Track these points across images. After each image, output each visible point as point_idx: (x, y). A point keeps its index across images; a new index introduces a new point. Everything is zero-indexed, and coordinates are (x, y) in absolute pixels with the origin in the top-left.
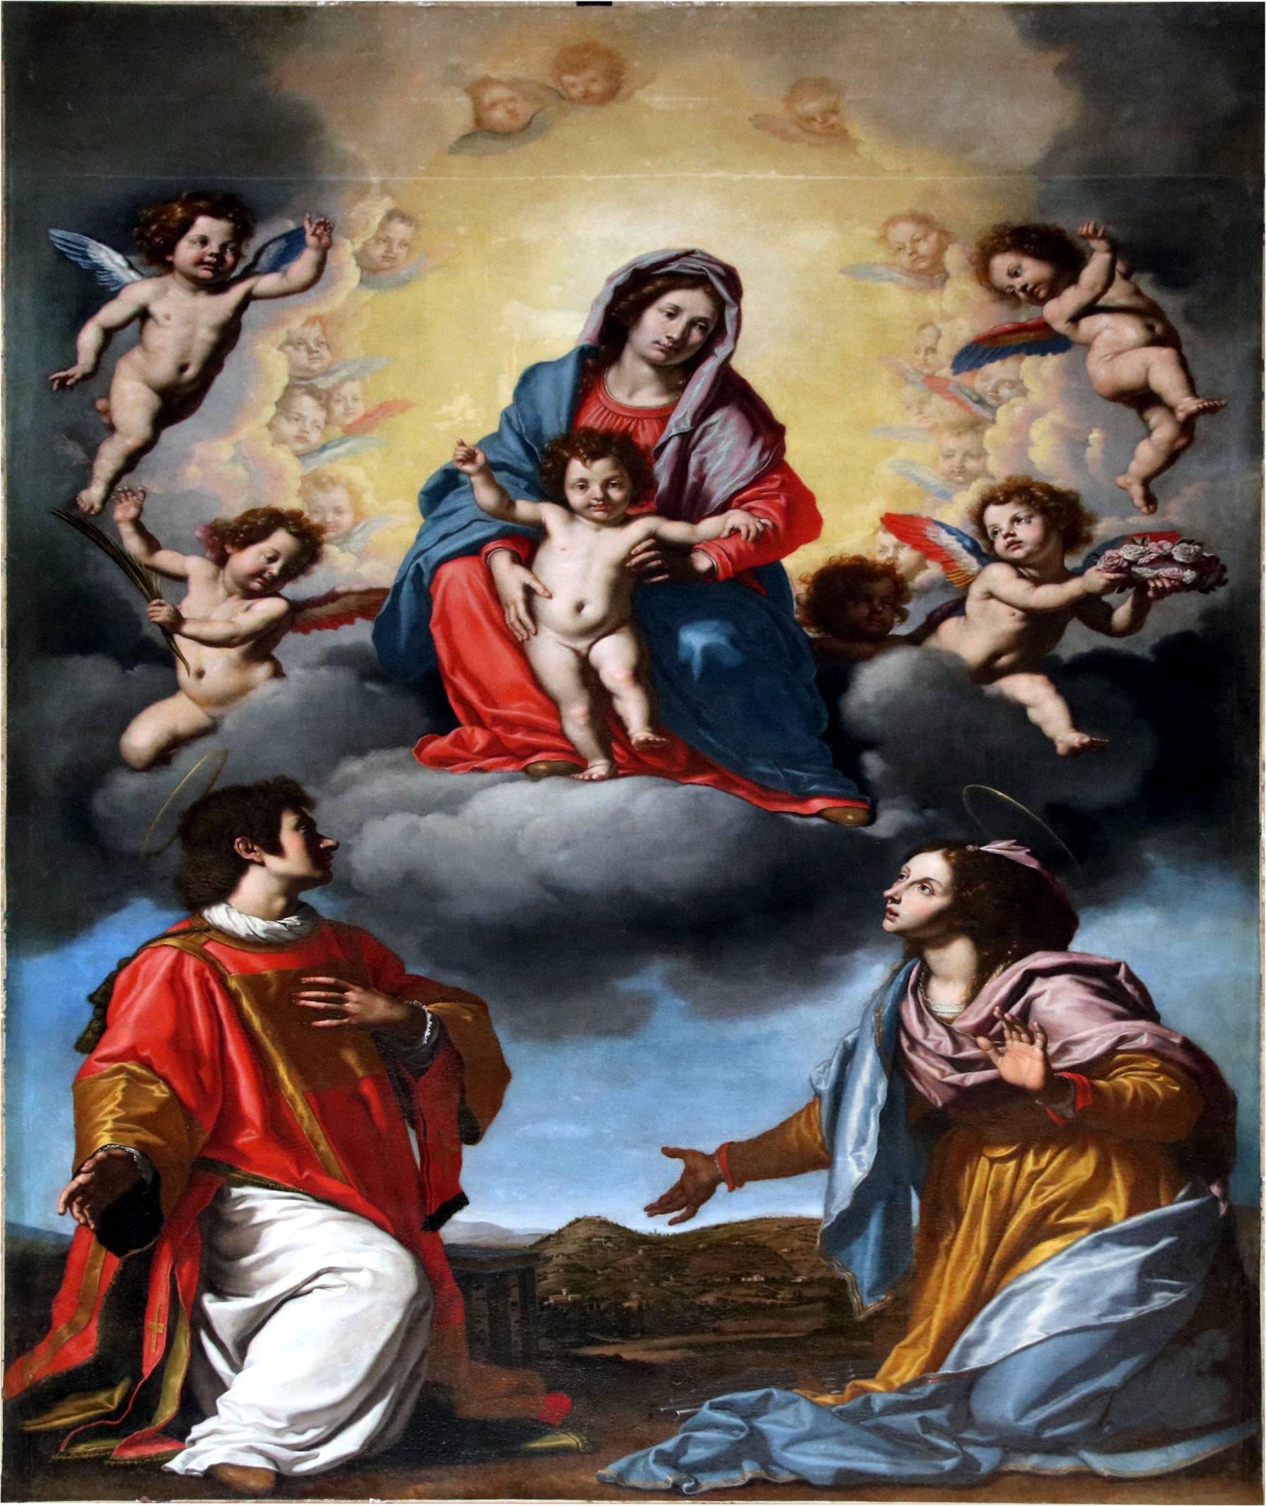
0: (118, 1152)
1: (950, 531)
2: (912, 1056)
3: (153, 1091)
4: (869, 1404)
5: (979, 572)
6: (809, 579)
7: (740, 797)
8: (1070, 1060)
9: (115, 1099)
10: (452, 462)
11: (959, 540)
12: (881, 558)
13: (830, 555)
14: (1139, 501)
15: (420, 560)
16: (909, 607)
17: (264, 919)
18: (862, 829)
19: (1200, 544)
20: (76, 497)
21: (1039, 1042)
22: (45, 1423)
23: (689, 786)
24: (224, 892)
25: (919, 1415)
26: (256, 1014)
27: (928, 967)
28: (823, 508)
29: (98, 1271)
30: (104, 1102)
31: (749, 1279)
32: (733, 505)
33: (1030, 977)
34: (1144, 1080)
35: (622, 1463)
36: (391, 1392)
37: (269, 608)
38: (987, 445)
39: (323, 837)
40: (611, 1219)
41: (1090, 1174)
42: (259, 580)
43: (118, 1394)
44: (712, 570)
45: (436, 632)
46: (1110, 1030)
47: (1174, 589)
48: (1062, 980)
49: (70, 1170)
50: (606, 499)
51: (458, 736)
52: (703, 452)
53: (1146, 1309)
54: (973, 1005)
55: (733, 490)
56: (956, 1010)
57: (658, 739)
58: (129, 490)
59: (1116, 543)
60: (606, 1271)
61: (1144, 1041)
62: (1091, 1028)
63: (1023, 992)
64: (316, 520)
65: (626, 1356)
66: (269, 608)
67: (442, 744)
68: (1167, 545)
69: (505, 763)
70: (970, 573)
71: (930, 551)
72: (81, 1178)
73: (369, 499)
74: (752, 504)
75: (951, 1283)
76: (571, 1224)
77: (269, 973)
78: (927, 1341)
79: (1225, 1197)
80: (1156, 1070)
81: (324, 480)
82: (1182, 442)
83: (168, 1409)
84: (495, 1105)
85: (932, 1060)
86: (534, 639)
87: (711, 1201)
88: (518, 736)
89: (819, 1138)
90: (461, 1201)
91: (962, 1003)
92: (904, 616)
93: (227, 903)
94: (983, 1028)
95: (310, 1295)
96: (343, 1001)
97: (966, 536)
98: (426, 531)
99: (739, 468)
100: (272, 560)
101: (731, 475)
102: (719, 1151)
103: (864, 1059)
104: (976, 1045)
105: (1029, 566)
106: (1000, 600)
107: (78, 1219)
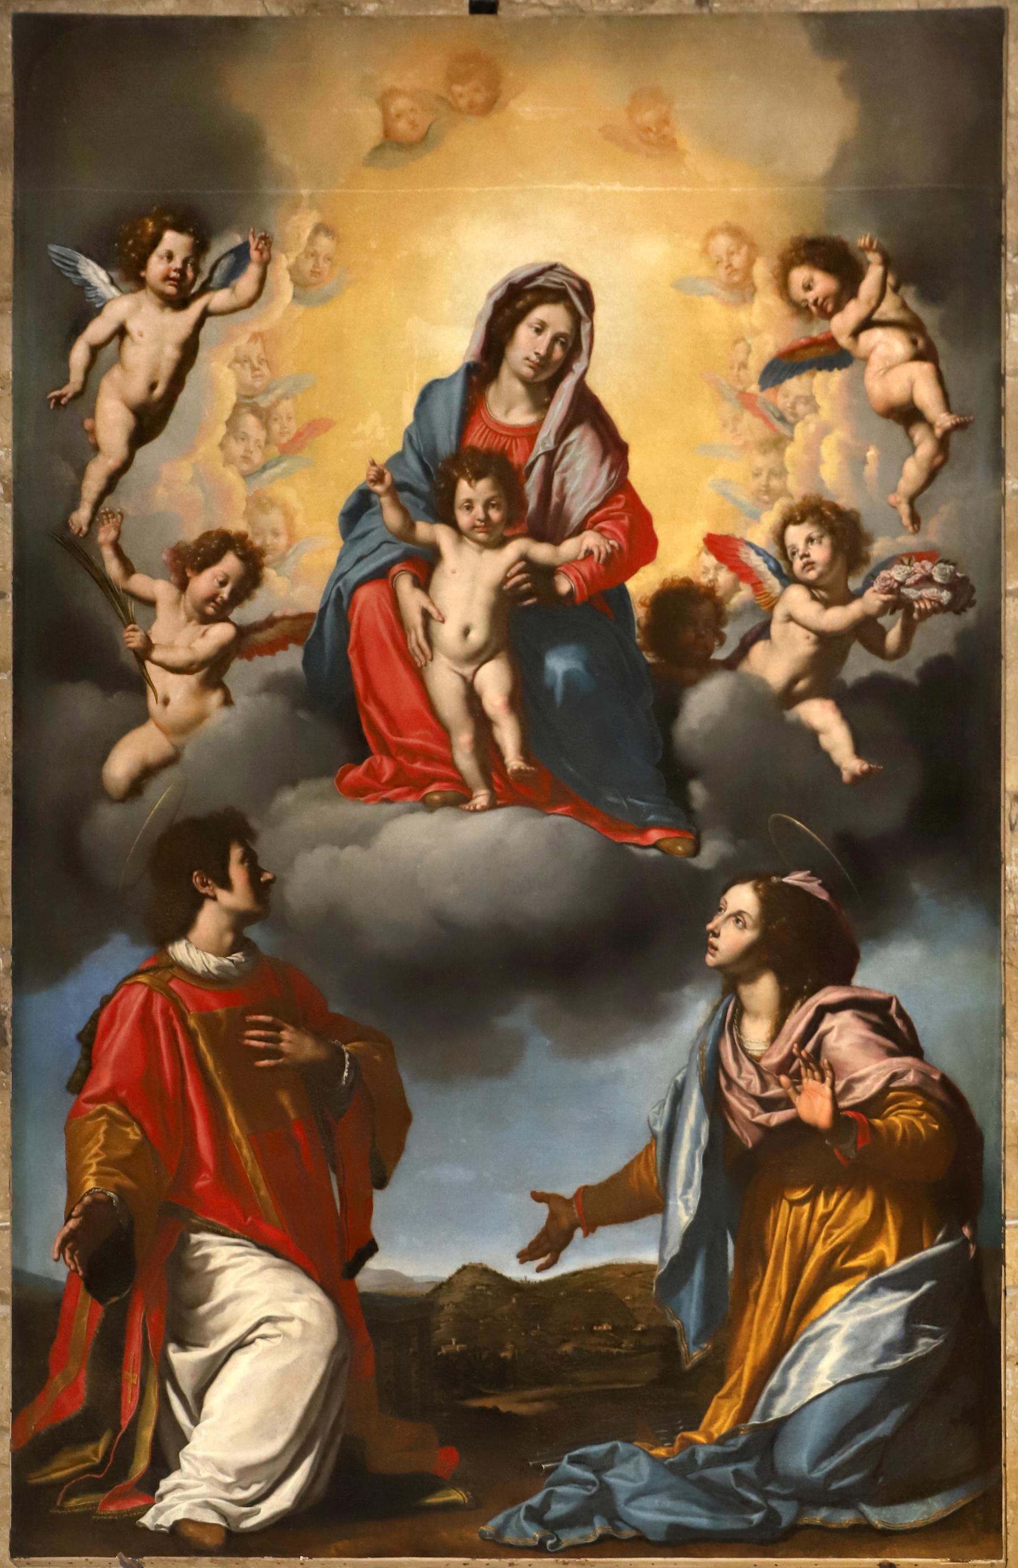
0: (100, 1196)
1: (759, 552)
3: (128, 1134)
5: (781, 594)
6: (648, 602)
8: (853, 1099)
10: (365, 483)
11: (766, 562)
12: (704, 580)
13: (664, 578)
14: (906, 520)
15: (340, 584)
16: (726, 630)
17: (217, 954)
19: (954, 564)
21: (828, 1080)
22: (45, 1475)
24: (183, 928)
26: (210, 1054)
28: (660, 529)
29: (85, 1319)
30: (90, 1144)
31: (600, 1328)
32: (587, 527)
33: (822, 1011)
35: (499, 1519)
39: (264, 871)
40: (492, 1266)
41: (868, 1217)
42: (212, 604)
43: (102, 1446)
44: (571, 593)
45: (353, 658)
46: (885, 1067)
47: (935, 611)
48: (846, 1016)
50: (487, 519)
51: (370, 764)
53: (912, 1355)
57: (528, 768)
58: (110, 512)
59: (887, 564)
61: (911, 1078)
63: (816, 1028)
64: (258, 542)
65: (504, 1408)
66: (221, 632)
67: (358, 772)
68: (928, 565)
69: (408, 794)
70: (773, 595)
71: (743, 573)
72: (72, 1223)
73: (299, 520)
74: (602, 525)
75: (759, 1330)
76: (459, 1272)
77: (220, 1011)
79: (974, 1238)
82: (939, 459)
83: (141, 1464)
84: (399, 1148)
85: (744, 1099)
86: (430, 664)
88: (418, 765)
89: (655, 1181)
90: (371, 1249)
92: (722, 639)
93: (186, 938)
94: (784, 1067)
95: (253, 1345)
97: (770, 556)
99: (592, 488)
100: (223, 584)
103: (691, 1098)
104: (779, 1084)
106: (798, 622)
107: (69, 1266)
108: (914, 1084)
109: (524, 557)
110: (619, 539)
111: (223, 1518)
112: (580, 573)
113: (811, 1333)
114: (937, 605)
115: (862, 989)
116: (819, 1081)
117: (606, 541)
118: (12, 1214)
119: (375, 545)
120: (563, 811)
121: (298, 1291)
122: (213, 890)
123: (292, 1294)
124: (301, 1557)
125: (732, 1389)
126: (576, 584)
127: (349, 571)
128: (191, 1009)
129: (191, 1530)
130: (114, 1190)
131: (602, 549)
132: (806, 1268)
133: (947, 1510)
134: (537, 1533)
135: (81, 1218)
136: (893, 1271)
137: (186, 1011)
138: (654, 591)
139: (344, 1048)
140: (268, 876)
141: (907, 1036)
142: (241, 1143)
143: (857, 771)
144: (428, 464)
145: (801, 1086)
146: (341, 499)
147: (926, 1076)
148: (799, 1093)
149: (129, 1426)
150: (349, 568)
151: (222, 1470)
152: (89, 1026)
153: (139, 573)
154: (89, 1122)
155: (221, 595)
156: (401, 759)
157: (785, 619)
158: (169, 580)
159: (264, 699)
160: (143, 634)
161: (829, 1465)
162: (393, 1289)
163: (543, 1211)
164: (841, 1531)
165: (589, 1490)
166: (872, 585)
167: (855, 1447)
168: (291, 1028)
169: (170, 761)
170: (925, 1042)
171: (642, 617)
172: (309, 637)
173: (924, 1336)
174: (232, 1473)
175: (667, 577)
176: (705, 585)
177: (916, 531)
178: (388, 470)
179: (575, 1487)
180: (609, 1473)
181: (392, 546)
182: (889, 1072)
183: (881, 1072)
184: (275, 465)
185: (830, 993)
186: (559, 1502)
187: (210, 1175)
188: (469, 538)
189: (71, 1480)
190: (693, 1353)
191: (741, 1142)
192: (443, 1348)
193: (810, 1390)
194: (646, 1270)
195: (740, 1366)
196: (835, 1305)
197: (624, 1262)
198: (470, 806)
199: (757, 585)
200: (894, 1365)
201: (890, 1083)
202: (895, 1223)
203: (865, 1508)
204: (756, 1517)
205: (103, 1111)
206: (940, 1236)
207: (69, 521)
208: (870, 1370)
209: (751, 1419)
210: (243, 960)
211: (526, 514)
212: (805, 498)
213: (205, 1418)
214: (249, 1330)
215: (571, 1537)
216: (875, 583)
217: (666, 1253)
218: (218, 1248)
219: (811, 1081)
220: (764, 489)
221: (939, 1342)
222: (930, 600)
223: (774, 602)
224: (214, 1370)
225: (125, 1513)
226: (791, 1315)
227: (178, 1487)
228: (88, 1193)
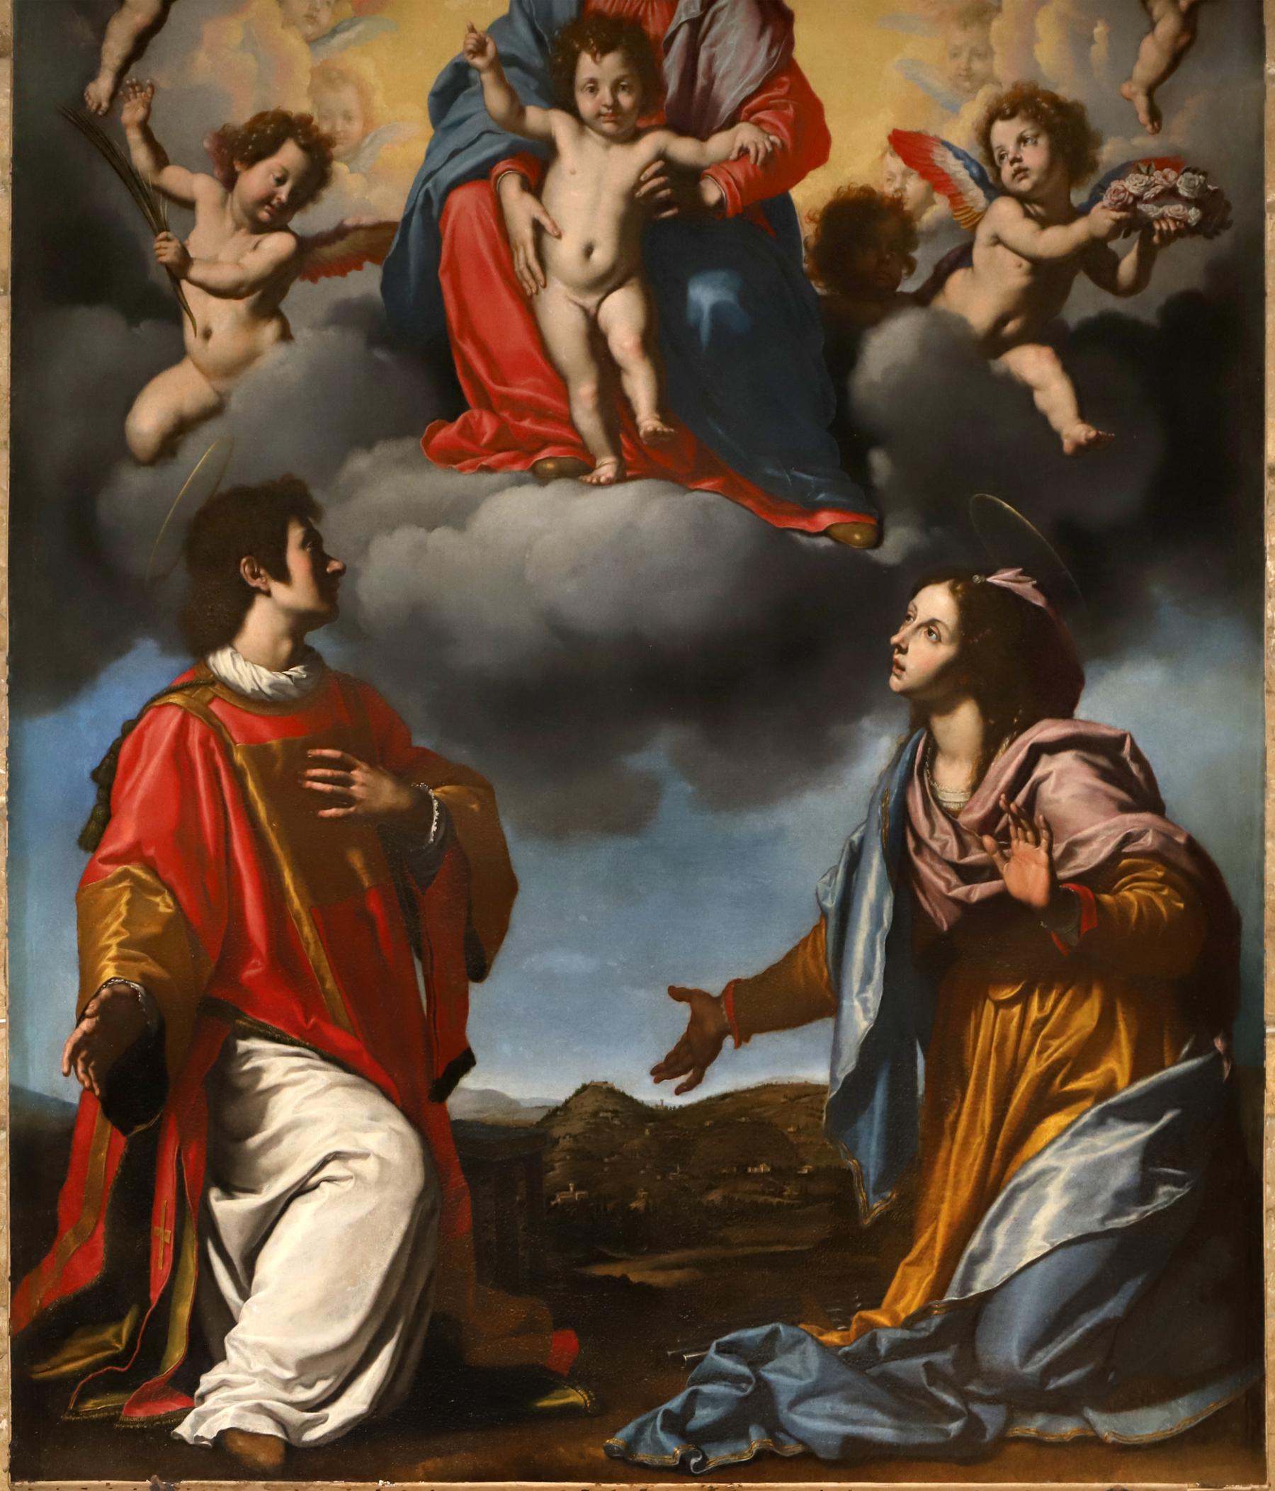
0: (123, 988)
1: (958, 155)
2: (918, 862)
3: (158, 905)
4: (875, 1344)
5: (986, 209)
6: (818, 216)
7: (746, 508)
8: (1075, 867)
9: (119, 915)
10: (462, 54)
11: (966, 167)
12: (889, 190)
13: (838, 185)
14: (1143, 117)
15: (429, 185)
16: (917, 254)
17: (269, 669)
18: (869, 552)
19: (1204, 174)
20: (83, 91)
21: (1044, 842)
22: (53, 1368)
23: (695, 493)
24: (227, 633)
25: (924, 1360)
26: (262, 800)
27: (934, 741)
28: (833, 123)
29: (103, 1154)
30: (109, 919)
31: (756, 1170)
32: (742, 118)
33: (1037, 752)
34: (1148, 894)
35: (629, 1430)
36: (400, 1327)
37: (277, 245)
38: (993, 41)
39: (332, 559)
40: (618, 1086)
41: (1094, 1024)
42: (267, 207)
43: (126, 1328)
44: (721, 203)
45: (445, 282)
46: (1115, 827)
47: (1179, 233)
48: (1067, 759)
49: (74, 1011)
50: (616, 105)
51: (466, 421)
52: (712, 45)
53: (1149, 1209)
54: (979, 791)
55: (741, 98)
56: (962, 799)
57: (666, 430)
58: (138, 84)
59: (1120, 172)
60: (613, 1159)
61: (1149, 841)
62: (1097, 823)
63: (1029, 775)
64: (325, 128)
65: (634, 1278)
66: (277, 245)
67: (450, 431)
68: (1172, 175)
69: (514, 461)
70: (976, 210)
71: (938, 181)
72: (86, 1025)
73: (378, 99)
74: (760, 115)
75: (957, 1174)
76: (578, 1093)
77: (274, 743)
78: (933, 1255)
79: (1228, 1049)
80: (1161, 880)
81: (334, 74)
82: (1183, 40)
83: (177, 1353)
84: (501, 928)
85: (938, 867)
86: (542, 292)
87: (716, 1061)
88: (526, 423)
89: (826, 974)
90: (466, 1061)
91: (968, 788)
92: (911, 266)
93: (232, 646)
94: (988, 824)
95: (317, 1191)
96: (348, 782)
97: (972, 161)
98: (490, 115)
99: (748, 67)
100: (281, 181)
101: (740, 78)
102: (725, 992)
103: (870, 865)
104: (982, 847)
105: (1037, 202)
106: (1006, 246)
107: (82, 1082)
108: (1153, 848)
109: (661, 156)
110: (783, 135)
111: (281, 1429)
112: (733, 178)
113: (1022, 1178)
114: (1182, 226)
115: (1087, 722)
116: (1032, 843)
117: (766, 136)
118: (8, 1012)
119: (473, 134)
120: (710, 487)
121: (374, 1118)
122: (265, 583)
123: (366, 1122)
124: (381, 1482)
125: (922, 1252)
126: (727, 190)
127: (439, 169)
128: (237, 741)
129: (240, 1443)
130: (139, 980)
131: (761, 146)
132: (1016, 1091)
133: (1196, 1417)
134: (679, 1448)
135: (98, 1018)
136: (1126, 1096)
137: (231, 742)
138: (826, 203)
139: (432, 793)
140: (335, 566)
141: (1145, 787)
142: (301, 918)
143: (1083, 440)
144: (542, 31)
145: (1010, 850)
146: (430, 75)
147: (1168, 838)
148: (1006, 859)
149: (160, 1300)
150: (440, 165)
151: (279, 1362)
152: (107, 760)
153: (173, 164)
154: (107, 890)
155: (278, 196)
156: (505, 414)
157: (992, 241)
158: (212, 175)
159: (331, 333)
160: (179, 245)
161: (1045, 1357)
162: (494, 1115)
163: (683, 1011)
164: (1061, 1445)
165: (744, 1390)
166: (1100, 199)
167: (1079, 1331)
168: (365, 767)
169: (213, 412)
170: (1168, 794)
171: (811, 236)
172: (390, 254)
173: (1165, 1184)
174: (292, 1366)
175: (843, 185)
176: (890, 196)
177: (1156, 131)
178: (491, 38)
179: (725, 1385)
180: (770, 1366)
181: (494, 137)
182: (1120, 833)
183: (1112, 832)
184: (348, 29)
185: (1047, 728)
186: (705, 1407)
187: (262, 961)
188: (591, 127)
189: (87, 1374)
190: (876, 1206)
191: (934, 924)
192: (558, 1196)
193: (1022, 1254)
194: (815, 1091)
195: (932, 1222)
196: (1052, 1141)
197: (786, 1082)
198: (592, 478)
199: (955, 197)
200: (1128, 1222)
201: (1123, 848)
202: (1129, 1032)
203: (1091, 1414)
204: (955, 1427)
205: (125, 875)
206: (1186, 1049)
207: (85, 94)
208: (1097, 1228)
209: (947, 1295)
210: (305, 676)
211: (665, 98)
212: (1015, 86)
213: (257, 1291)
214: (312, 1170)
215: (720, 1454)
216: (1105, 197)
217: (839, 1069)
218: (273, 1059)
219: (1022, 843)
220: (964, 73)
221: (1184, 1191)
222: (1174, 220)
223: (977, 219)
224: (268, 1225)
225: (157, 1420)
226: (998, 1152)
227: (223, 1384)
228: (106, 984)
